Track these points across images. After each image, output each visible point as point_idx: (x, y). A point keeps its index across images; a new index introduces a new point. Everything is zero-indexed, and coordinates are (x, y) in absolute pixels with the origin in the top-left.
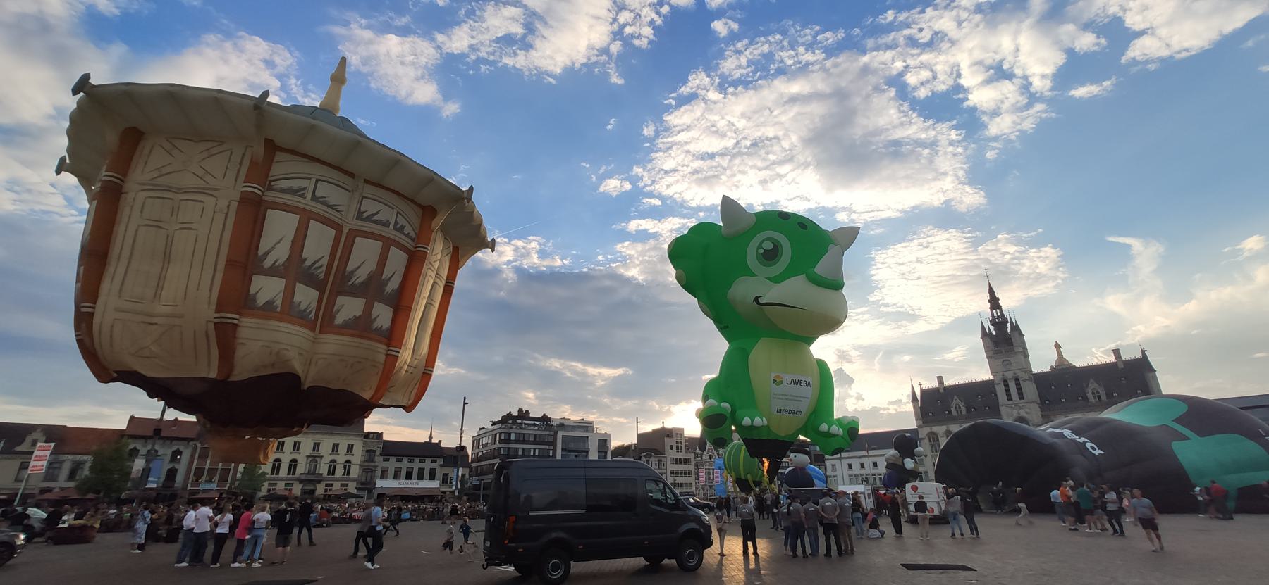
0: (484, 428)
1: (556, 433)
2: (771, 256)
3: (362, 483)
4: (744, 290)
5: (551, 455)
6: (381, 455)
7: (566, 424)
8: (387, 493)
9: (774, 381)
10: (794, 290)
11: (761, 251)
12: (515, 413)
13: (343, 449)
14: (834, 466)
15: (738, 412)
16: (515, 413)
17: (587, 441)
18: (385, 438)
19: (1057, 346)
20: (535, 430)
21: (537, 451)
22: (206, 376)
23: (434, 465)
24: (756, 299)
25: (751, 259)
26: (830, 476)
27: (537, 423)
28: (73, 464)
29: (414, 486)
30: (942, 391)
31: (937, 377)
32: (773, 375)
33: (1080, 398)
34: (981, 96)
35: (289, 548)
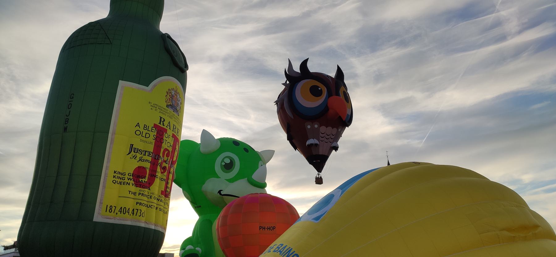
2: (228, 167)
11: (223, 164)
19: (135, 127)
25: (218, 168)
28: (277, 104)
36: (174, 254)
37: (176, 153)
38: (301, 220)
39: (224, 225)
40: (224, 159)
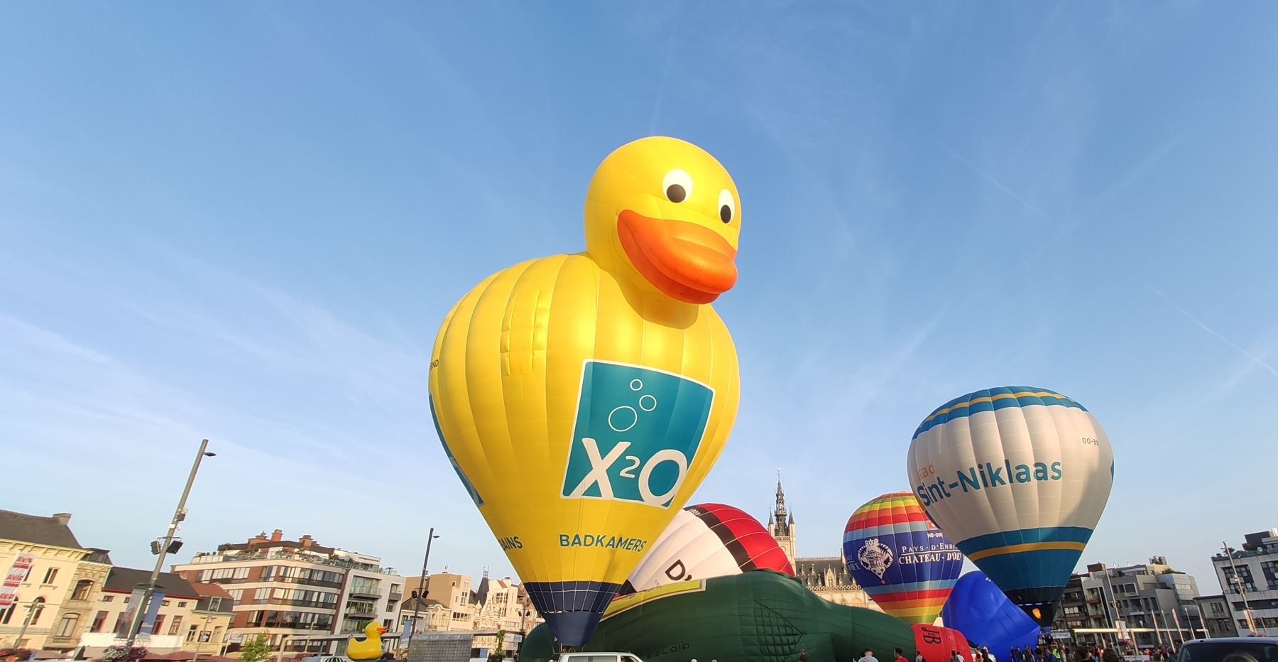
3: (57, 639)
6: (104, 590)
13: (38, 573)
21: (322, 595)
23: (181, 611)
31: (70, 515)
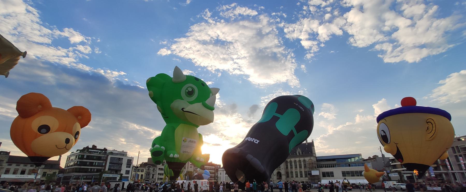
0: (73, 152)
1: (108, 156)
2: (190, 93)
4: (178, 104)
5: (104, 165)
6: (7, 162)
7: (113, 152)
8: (7, 180)
9: (184, 141)
10: (196, 108)
11: (187, 91)
12: (91, 147)
14: (221, 173)
15: (168, 152)
16: (91, 147)
17: (122, 160)
18: (11, 154)
20: (98, 154)
21: (97, 163)
22: (216, 98)
24: (183, 109)
25: (183, 93)
26: (219, 177)
27: (99, 151)
29: (25, 178)
30: (307, 144)
32: (183, 139)
33: (295, 154)
34: (306, 44)
35: (463, 185)
36: (275, 111)
37: (451, 163)
38: (250, 124)
39: (124, 144)
40: (188, 88)
